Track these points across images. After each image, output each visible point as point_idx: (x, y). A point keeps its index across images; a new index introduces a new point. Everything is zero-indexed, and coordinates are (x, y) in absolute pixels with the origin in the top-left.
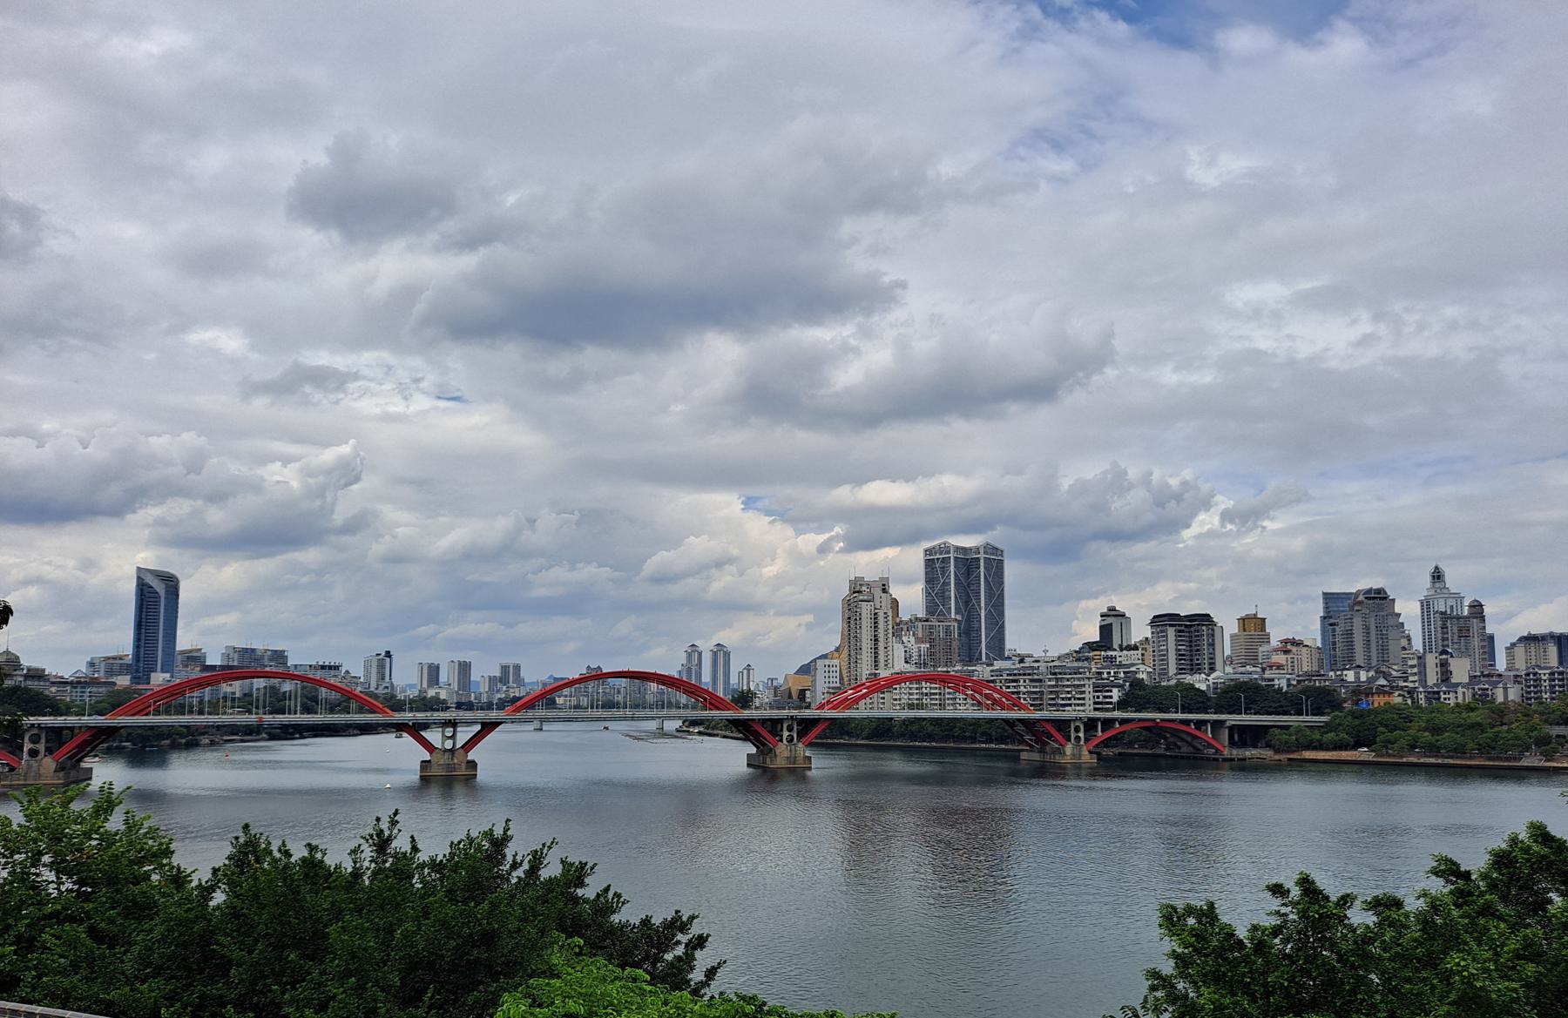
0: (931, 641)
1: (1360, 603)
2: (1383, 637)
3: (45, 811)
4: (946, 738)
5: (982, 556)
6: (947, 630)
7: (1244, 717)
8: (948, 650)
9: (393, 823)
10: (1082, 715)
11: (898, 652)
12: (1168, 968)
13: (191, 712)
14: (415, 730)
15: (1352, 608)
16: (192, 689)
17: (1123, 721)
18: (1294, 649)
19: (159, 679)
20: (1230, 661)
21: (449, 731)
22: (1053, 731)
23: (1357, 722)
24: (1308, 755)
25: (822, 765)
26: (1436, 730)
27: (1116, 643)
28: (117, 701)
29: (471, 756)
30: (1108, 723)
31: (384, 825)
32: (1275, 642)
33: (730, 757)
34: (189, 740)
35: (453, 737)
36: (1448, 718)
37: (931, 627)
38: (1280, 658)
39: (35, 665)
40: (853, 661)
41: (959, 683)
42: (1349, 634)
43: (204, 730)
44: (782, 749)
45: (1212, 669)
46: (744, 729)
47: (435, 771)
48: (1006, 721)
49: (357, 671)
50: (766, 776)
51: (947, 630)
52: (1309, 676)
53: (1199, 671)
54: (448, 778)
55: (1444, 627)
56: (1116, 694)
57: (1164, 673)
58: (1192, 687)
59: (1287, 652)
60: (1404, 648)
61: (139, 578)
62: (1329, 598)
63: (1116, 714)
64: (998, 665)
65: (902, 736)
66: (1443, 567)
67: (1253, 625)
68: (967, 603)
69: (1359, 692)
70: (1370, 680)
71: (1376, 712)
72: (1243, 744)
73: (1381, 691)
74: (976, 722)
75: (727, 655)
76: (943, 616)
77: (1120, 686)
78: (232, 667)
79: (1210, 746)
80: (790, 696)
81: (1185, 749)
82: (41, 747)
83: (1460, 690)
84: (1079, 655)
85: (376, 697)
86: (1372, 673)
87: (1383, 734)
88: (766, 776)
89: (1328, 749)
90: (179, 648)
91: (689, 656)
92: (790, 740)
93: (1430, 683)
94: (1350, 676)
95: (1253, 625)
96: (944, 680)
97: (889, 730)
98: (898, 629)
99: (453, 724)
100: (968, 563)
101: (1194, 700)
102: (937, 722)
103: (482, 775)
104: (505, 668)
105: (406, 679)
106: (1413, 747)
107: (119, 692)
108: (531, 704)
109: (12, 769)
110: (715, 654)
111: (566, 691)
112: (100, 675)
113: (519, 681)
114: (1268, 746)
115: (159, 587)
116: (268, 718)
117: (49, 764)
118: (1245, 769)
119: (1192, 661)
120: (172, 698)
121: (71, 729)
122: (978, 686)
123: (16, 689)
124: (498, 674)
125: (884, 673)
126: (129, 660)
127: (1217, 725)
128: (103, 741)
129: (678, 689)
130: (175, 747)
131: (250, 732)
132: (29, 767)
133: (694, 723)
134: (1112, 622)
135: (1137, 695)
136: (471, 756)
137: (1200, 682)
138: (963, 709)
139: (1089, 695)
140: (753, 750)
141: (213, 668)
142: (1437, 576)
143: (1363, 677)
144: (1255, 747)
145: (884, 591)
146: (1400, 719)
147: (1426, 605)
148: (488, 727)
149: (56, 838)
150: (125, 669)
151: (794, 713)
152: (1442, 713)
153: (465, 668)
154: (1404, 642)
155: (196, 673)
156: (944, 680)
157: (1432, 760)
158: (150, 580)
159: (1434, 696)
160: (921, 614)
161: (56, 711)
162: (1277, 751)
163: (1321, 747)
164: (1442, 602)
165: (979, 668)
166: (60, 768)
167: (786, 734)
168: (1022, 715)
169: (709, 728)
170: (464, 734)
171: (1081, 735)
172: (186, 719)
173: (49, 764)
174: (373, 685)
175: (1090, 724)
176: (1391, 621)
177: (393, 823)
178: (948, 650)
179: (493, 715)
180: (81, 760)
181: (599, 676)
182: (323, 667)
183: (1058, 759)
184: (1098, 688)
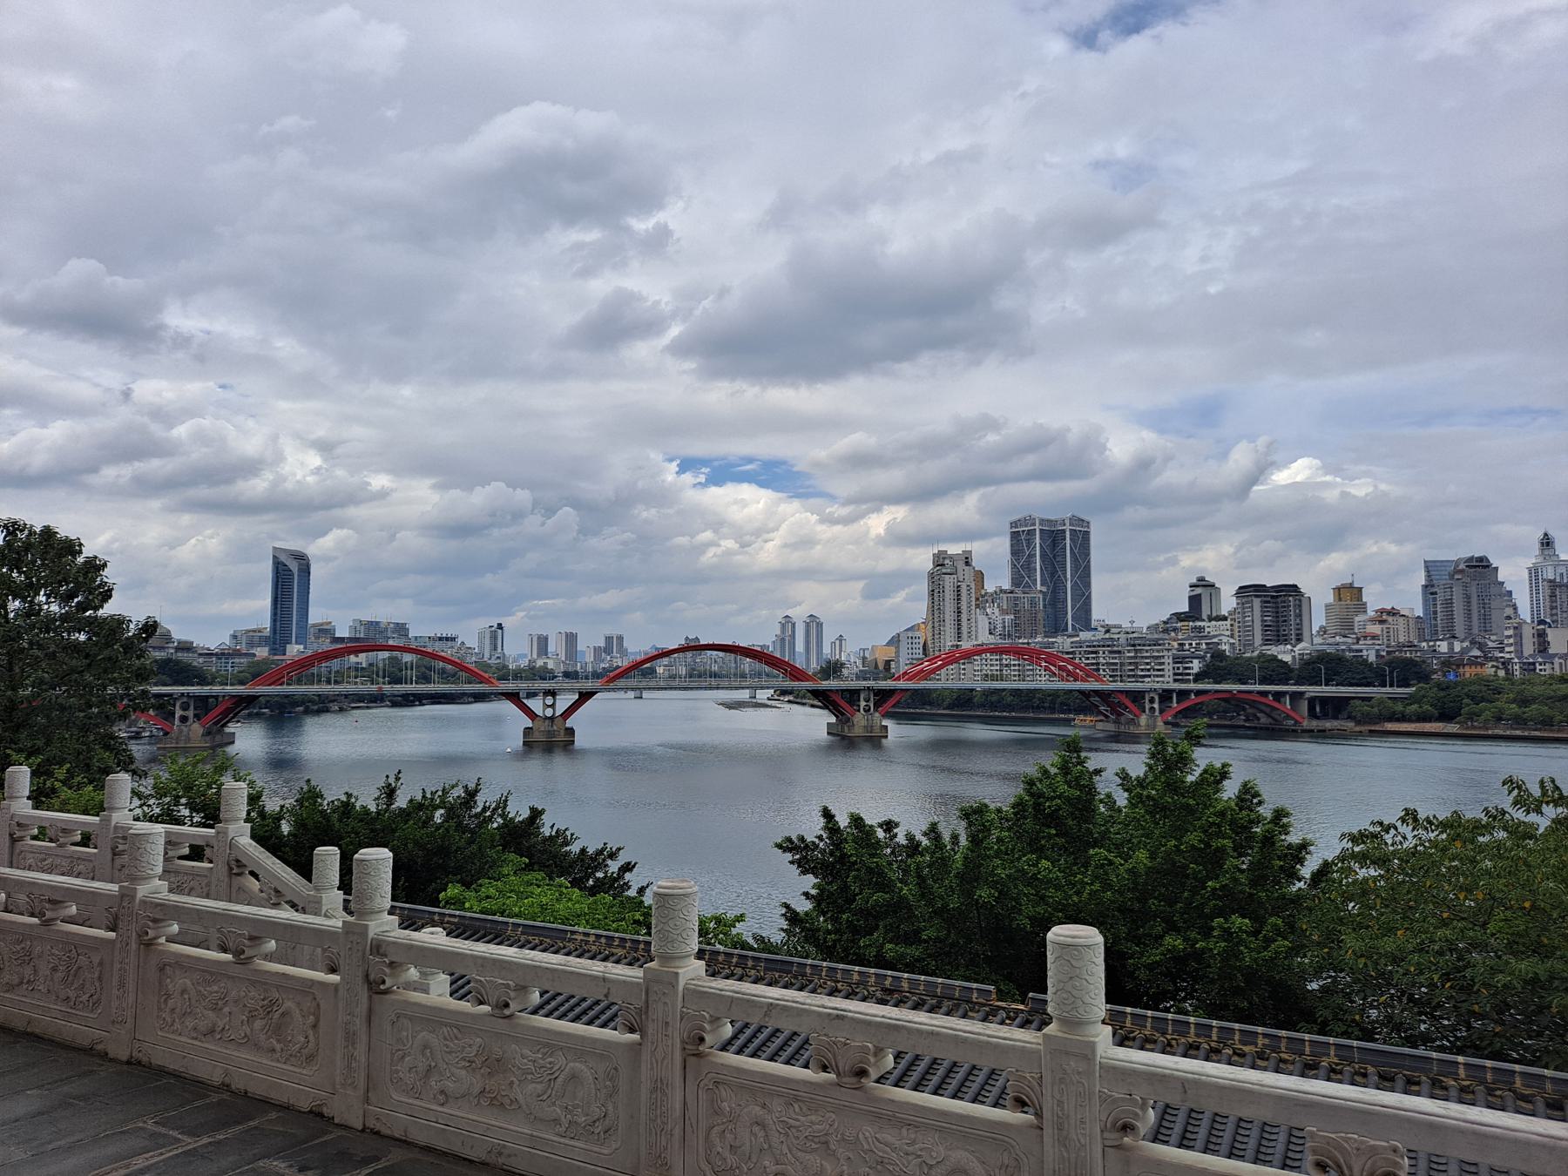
0: (1016, 612)
1: (1462, 571)
2: (1484, 605)
3: (182, 769)
4: (1025, 709)
5: (1068, 527)
6: (1033, 603)
7: (1324, 688)
8: (1034, 620)
9: (398, 779)
10: (1157, 686)
11: (983, 623)
12: (803, 906)
13: (319, 681)
14: (514, 697)
15: (1451, 577)
16: (320, 662)
17: (1199, 693)
18: (1390, 619)
19: (294, 650)
20: (1323, 631)
21: (549, 701)
22: (1128, 702)
23: (1442, 694)
24: (1390, 726)
25: (896, 732)
26: (1524, 702)
27: (1205, 612)
28: (257, 673)
29: (569, 723)
30: (1183, 694)
31: (392, 780)
32: (1371, 613)
33: (815, 723)
34: (320, 706)
35: (553, 706)
36: (1537, 690)
37: (1016, 599)
38: (1376, 629)
39: (184, 638)
40: (937, 632)
41: (1033, 655)
42: (1449, 603)
43: (334, 698)
44: (860, 719)
45: (1299, 640)
46: (824, 699)
47: (537, 737)
48: (1081, 692)
49: (472, 643)
50: (844, 741)
51: (1033, 603)
52: (1401, 646)
53: (1286, 642)
54: (550, 740)
55: (1553, 595)
56: (1196, 666)
57: (1249, 644)
58: (1274, 658)
59: (1382, 622)
60: (1509, 618)
61: (275, 557)
62: (1429, 567)
63: (1192, 686)
64: (1085, 635)
65: (982, 706)
66: (1551, 533)
67: (1349, 594)
68: (1052, 575)
69: (1449, 663)
70: (1464, 651)
71: (1464, 684)
72: (1325, 716)
73: (1473, 662)
74: (1055, 694)
75: (820, 625)
76: (1028, 588)
77: (1202, 658)
78: (356, 640)
79: (1288, 717)
80: (876, 667)
81: (1264, 720)
82: (190, 713)
83: (1556, 660)
84: (1167, 627)
85: (489, 666)
86: (1466, 644)
87: (1468, 706)
88: (844, 741)
89: (1410, 721)
90: (311, 621)
91: (783, 626)
92: (184, 719)
93: (1526, 654)
94: (1443, 647)
95: (1349, 594)
96: (1018, 652)
97: (970, 700)
98: (982, 601)
99: (552, 693)
100: (1053, 537)
101: (1275, 671)
102: (1016, 692)
103: (580, 741)
104: (609, 639)
105: (517, 651)
106: (1500, 719)
107: (258, 663)
108: (625, 673)
109: (166, 734)
110: (808, 625)
111: (665, 661)
112: (242, 647)
113: (623, 652)
114: (1350, 717)
115: (294, 566)
116: (387, 688)
117: (197, 729)
118: (1321, 736)
119: (1277, 634)
120: (303, 667)
121: (216, 697)
122: (1051, 659)
123: (168, 661)
124: (602, 644)
125: (966, 645)
126: (267, 632)
127: (1296, 696)
128: (243, 707)
129: (760, 661)
130: (307, 712)
131: (376, 699)
132: (181, 731)
133: (784, 693)
134: (1202, 591)
135: (1218, 667)
136: (569, 723)
137: (1285, 654)
138: (1041, 680)
139: (1169, 668)
140: (833, 719)
141: (342, 640)
142: (1547, 543)
143: (1457, 648)
144: (1336, 718)
145: (967, 564)
146: (1490, 690)
147: (1534, 572)
148: (585, 696)
149: (188, 788)
150: (264, 641)
151: (871, 683)
152: (1533, 684)
153: (571, 639)
154: (1509, 611)
155: (326, 645)
156: (1018, 652)
157: (1518, 733)
158: (283, 558)
159: (1529, 667)
160: (1007, 586)
161: (203, 681)
162: (1358, 723)
163: (1403, 718)
164: (1550, 570)
165: (1059, 639)
166: (208, 733)
167: (863, 704)
168: (1096, 686)
169: (798, 698)
170: (564, 702)
171: (1156, 706)
172: (315, 689)
173: (197, 729)
174: (487, 655)
175: (1165, 696)
176: (1494, 590)
177: (398, 779)
178: (1034, 620)
179: (589, 685)
180: (225, 725)
181: (694, 647)
182: (440, 639)
183: (1132, 729)
184: (1178, 660)
